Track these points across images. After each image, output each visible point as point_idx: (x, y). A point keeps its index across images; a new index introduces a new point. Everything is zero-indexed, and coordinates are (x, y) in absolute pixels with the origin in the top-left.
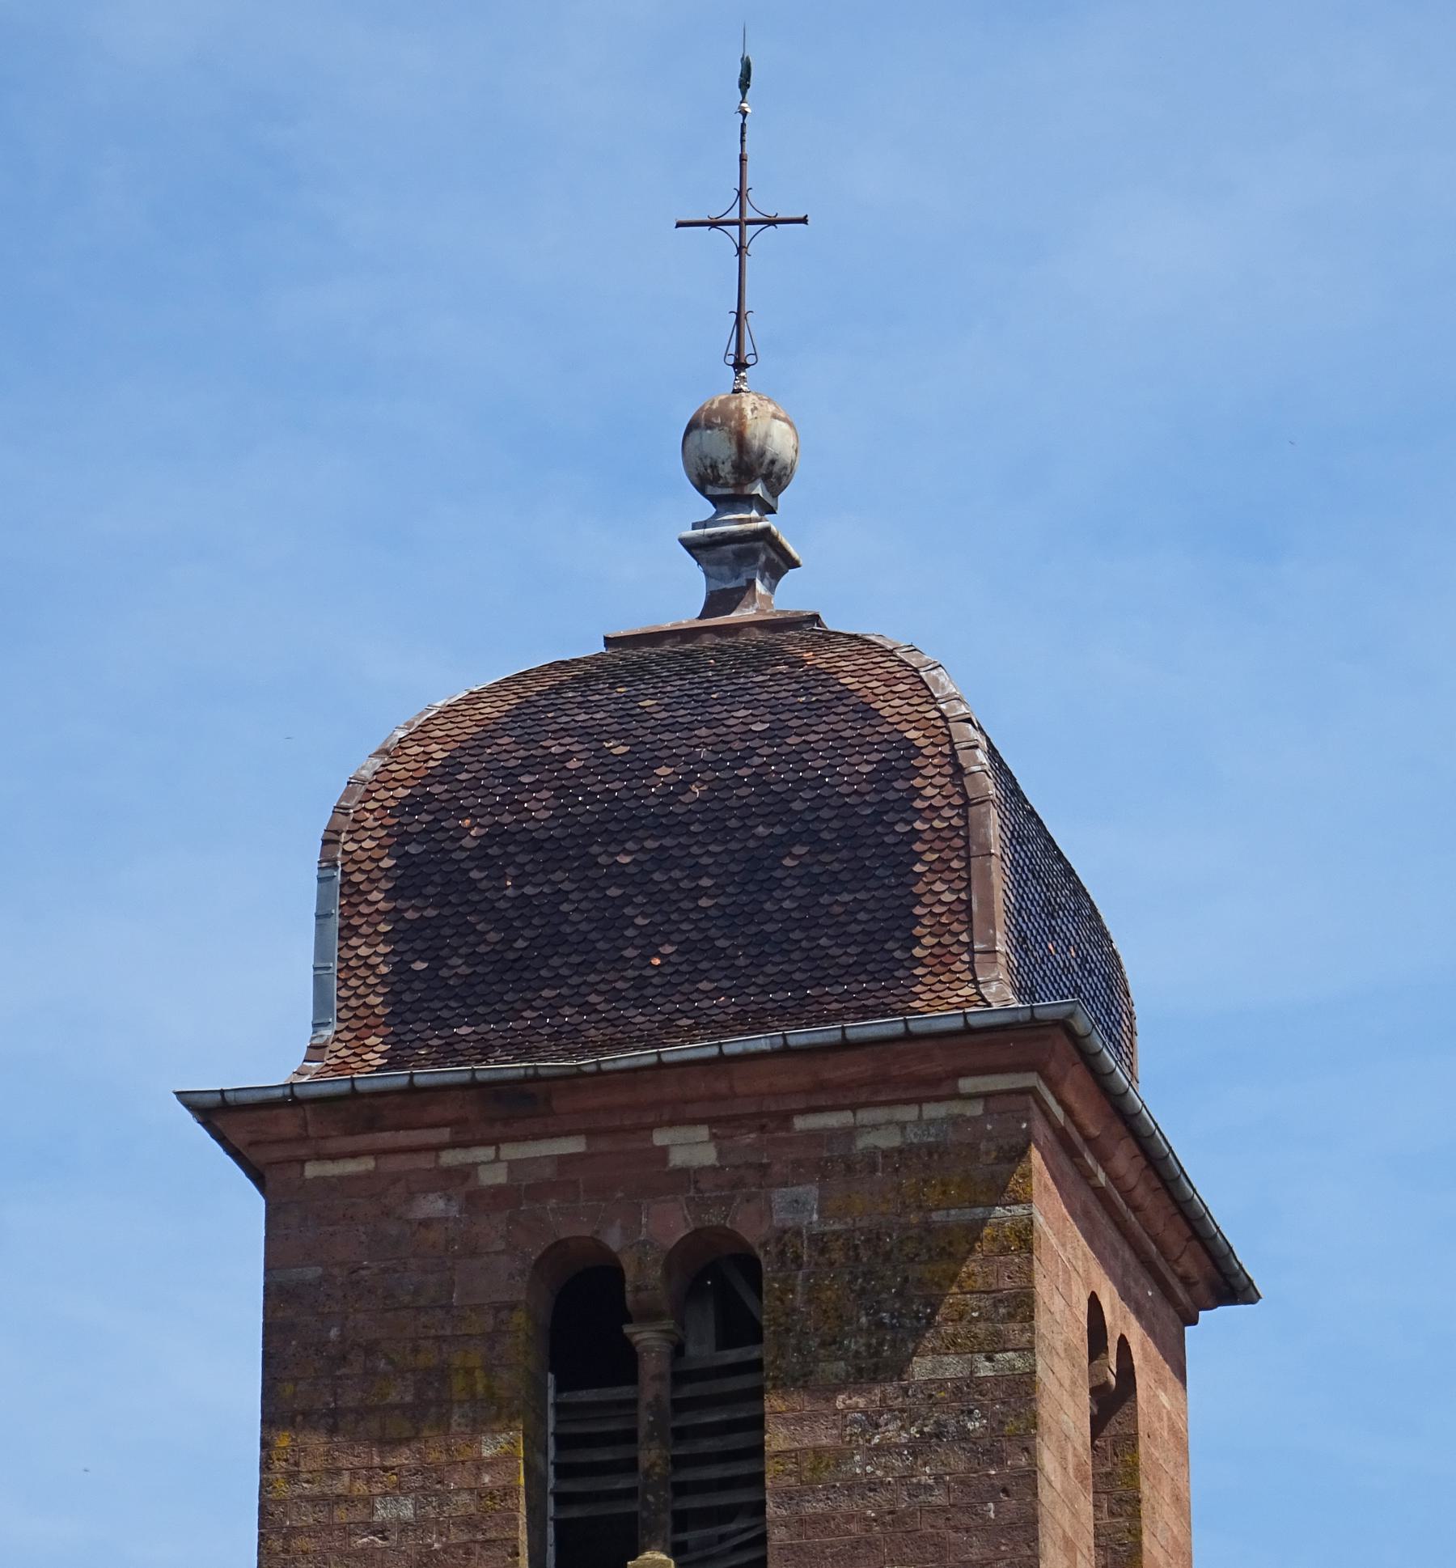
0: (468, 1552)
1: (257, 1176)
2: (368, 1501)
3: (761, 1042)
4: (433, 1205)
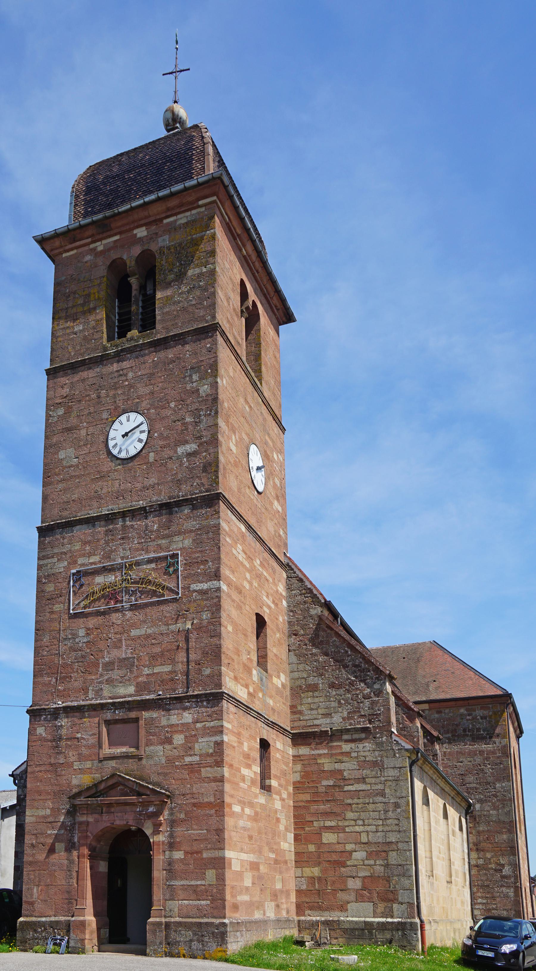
0: (93, 335)
1: (53, 261)
2: (73, 327)
3: (153, 197)
4: (88, 258)
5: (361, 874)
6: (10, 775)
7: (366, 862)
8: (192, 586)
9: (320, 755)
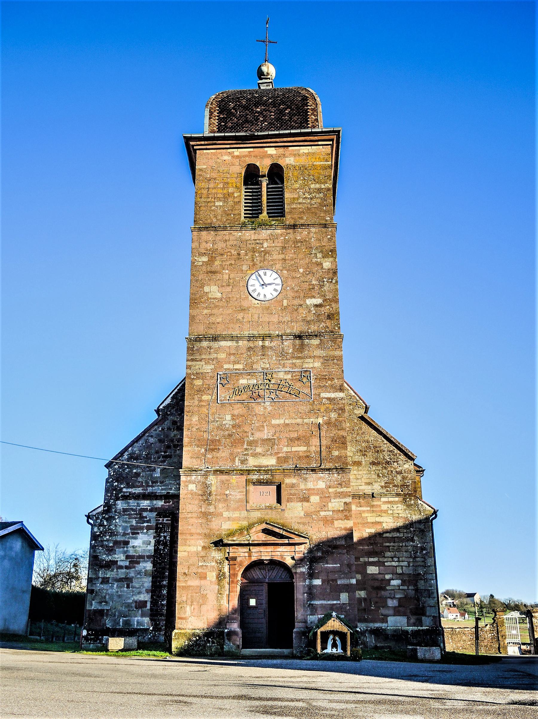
2: (214, 202)
5: (398, 596)
6: (86, 516)
7: (401, 587)
8: (321, 394)
9: (364, 511)
